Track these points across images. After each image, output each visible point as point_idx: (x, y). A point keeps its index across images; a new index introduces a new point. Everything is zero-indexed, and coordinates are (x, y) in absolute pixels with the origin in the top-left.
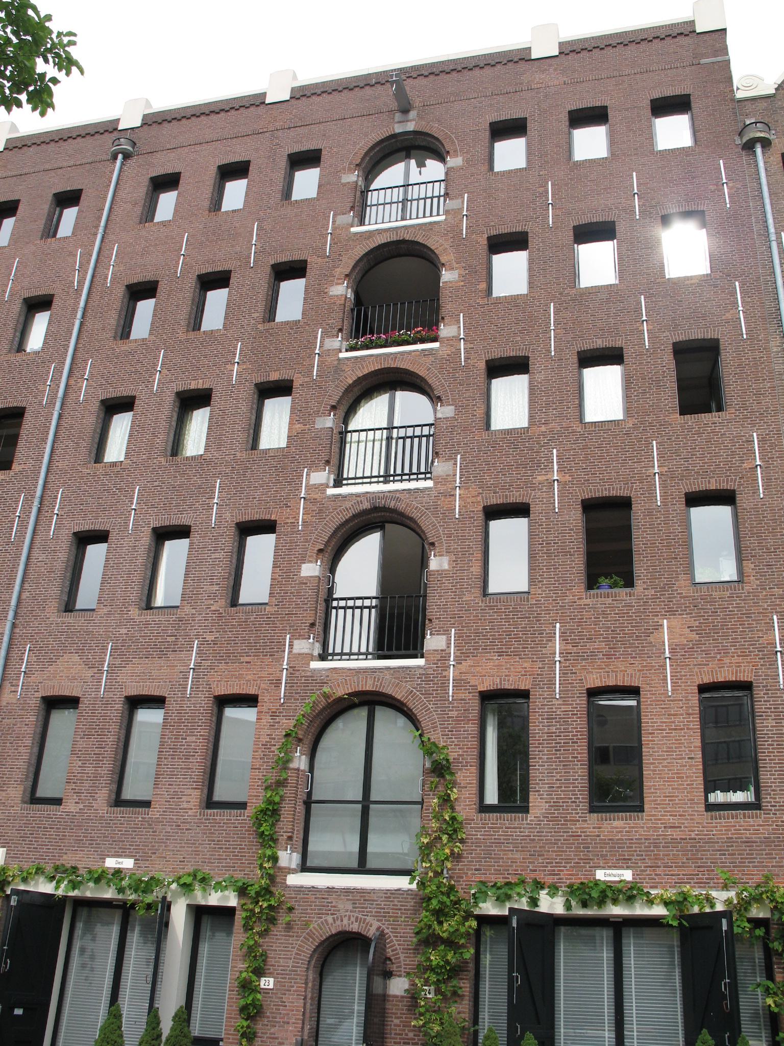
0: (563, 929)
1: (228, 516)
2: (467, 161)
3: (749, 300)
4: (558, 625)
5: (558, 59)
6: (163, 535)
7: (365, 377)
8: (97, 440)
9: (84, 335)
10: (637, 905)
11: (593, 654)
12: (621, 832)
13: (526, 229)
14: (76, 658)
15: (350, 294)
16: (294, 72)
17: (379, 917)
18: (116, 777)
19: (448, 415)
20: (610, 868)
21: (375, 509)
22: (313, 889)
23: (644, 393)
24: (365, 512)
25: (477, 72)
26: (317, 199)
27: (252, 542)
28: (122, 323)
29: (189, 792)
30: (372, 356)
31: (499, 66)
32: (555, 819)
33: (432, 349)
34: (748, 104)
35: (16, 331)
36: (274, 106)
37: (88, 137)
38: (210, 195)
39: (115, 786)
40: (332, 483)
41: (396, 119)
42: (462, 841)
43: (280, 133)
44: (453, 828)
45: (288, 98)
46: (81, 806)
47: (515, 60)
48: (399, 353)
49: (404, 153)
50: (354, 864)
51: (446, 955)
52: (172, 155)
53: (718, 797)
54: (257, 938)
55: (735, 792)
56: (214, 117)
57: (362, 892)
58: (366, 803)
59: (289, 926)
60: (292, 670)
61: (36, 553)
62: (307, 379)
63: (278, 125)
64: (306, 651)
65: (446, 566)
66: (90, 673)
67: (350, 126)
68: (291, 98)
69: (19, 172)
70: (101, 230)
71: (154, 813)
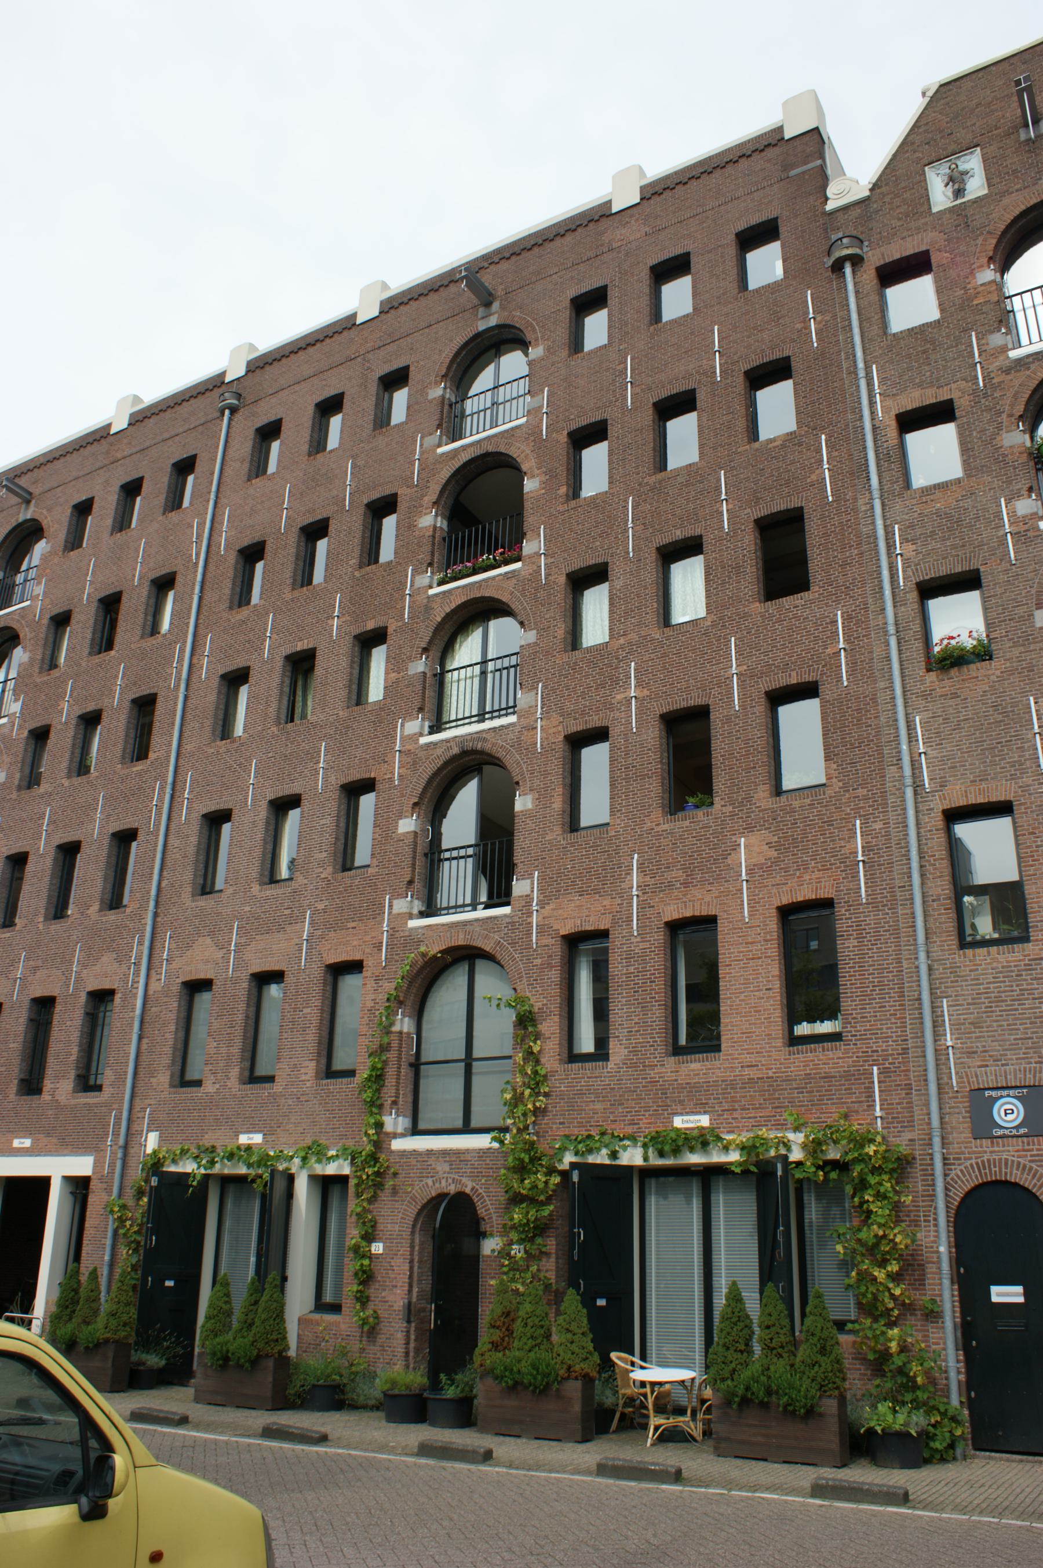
0: (653, 1181)
1: (332, 779)
2: (548, 349)
3: (837, 454)
4: (636, 856)
5: (639, 207)
6: (578, 741)
7: (454, 612)
8: (221, 717)
9: (204, 609)
10: (714, 1152)
11: (670, 885)
12: (698, 1074)
13: (605, 416)
14: (208, 940)
15: (441, 523)
16: (640, 168)
17: (473, 1177)
18: (248, 1055)
19: (530, 641)
20: (687, 1114)
21: (465, 753)
22: (414, 1153)
23: (724, 583)
24: (454, 758)
25: (558, 242)
26: (406, 423)
27: (787, 712)
28: (238, 590)
29: (307, 1063)
30: (458, 588)
31: (579, 230)
32: (634, 1066)
33: (514, 571)
34: (840, 214)
35: (146, 614)
36: (365, 326)
37: (200, 396)
38: (309, 438)
39: (247, 1064)
40: (426, 730)
41: (480, 315)
42: (546, 1095)
43: (370, 356)
44: (536, 1082)
45: (638, 201)
46: (217, 1086)
47: (596, 218)
48: (484, 580)
49: (493, 351)
50: (459, 1123)
51: (528, 1213)
52: (274, 400)
53: (803, 1029)
54: (365, 1204)
55: (822, 1021)
56: (311, 350)
57: (458, 1153)
58: (469, 1061)
59: (395, 1191)
60: (393, 931)
61: (173, 841)
62: (400, 624)
63: (369, 345)
64: (404, 910)
65: (530, 806)
66: (221, 954)
67: (436, 333)
68: (380, 313)
69: (142, 447)
70: (213, 496)
71: (278, 1087)
